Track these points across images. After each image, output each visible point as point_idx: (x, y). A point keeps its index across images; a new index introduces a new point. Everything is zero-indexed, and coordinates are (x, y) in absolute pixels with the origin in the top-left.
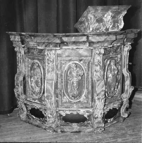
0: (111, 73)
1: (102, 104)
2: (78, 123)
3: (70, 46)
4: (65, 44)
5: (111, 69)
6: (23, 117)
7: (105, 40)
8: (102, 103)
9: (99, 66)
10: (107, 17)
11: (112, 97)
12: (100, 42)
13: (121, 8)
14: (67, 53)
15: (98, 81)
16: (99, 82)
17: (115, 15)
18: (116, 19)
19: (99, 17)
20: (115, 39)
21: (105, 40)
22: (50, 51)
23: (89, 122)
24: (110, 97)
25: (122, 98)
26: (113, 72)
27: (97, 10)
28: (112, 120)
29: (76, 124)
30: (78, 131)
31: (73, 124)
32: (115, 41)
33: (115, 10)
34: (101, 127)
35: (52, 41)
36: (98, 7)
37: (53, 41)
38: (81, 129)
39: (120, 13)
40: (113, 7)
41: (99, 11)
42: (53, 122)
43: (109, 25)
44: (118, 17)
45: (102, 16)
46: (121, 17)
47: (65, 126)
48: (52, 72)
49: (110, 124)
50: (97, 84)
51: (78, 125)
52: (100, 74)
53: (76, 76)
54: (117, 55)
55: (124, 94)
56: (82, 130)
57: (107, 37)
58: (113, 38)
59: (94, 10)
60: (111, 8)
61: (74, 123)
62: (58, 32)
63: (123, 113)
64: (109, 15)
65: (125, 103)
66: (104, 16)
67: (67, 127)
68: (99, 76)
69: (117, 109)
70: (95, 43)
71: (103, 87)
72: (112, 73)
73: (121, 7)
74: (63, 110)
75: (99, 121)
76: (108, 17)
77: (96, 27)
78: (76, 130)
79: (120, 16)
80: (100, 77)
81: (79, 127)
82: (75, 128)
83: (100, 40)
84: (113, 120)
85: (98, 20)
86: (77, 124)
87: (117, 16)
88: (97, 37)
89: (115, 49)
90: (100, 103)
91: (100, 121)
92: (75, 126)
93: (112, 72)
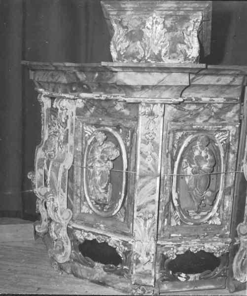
0: (191, 167)
1: (147, 232)
2: (105, 264)
3: (94, 93)
4: (84, 88)
5: (191, 156)
6: (40, 230)
7: (160, 84)
8: (147, 229)
9: (150, 144)
10: (154, 28)
11: (195, 224)
12: (147, 87)
13: (186, 7)
14: (93, 109)
15: (141, 177)
16: (144, 180)
17: (175, 24)
18: (179, 32)
19: (133, 27)
20: (188, 84)
21: (159, 83)
22: (84, 103)
23: (125, 267)
24: (192, 224)
25: (239, 234)
26: (196, 165)
27: (123, 11)
28: (195, 278)
29: (101, 265)
30: (101, 281)
31: (96, 264)
32: (187, 87)
33: (171, 12)
34: (143, 286)
35: (57, 80)
36: (124, 4)
37: (58, 79)
38: (108, 279)
39: (185, 18)
40: (161, 3)
41: (129, 13)
42: (60, 250)
43: (160, 48)
44: (184, 28)
45: (141, 24)
46: (190, 29)
47: (82, 264)
48: (64, 146)
49: (188, 286)
50: (139, 184)
51: (104, 268)
52: (152, 164)
53: (100, 160)
54: (221, 127)
55: (242, 224)
56: (108, 281)
57: (165, 78)
58: (184, 80)
59: (115, 11)
60: (158, 7)
61: (98, 262)
62: (86, 62)
63: (237, 270)
64: (156, 22)
65: (243, 247)
66: (144, 24)
67: (85, 267)
68: (150, 166)
69: (215, 257)
70: (135, 90)
71: (153, 194)
72: (193, 166)
73: (185, 5)
74: (81, 230)
75: (146, 271)
76: (156, 28)
77: (125, 51)
78: (97, 279)
79: (188, 27)
80: (152, 169)
81: (105, 273)
82: (97, 272)
83: (146, 83)
84: (197, 279)
85: (132, 34)
86: (104, 265)
87: (181, 27)
88: (139, 74)
89: (215, 110)
90: (143, 228)
91: (148, 272)
92: (99, 270)
93: (194, 164)
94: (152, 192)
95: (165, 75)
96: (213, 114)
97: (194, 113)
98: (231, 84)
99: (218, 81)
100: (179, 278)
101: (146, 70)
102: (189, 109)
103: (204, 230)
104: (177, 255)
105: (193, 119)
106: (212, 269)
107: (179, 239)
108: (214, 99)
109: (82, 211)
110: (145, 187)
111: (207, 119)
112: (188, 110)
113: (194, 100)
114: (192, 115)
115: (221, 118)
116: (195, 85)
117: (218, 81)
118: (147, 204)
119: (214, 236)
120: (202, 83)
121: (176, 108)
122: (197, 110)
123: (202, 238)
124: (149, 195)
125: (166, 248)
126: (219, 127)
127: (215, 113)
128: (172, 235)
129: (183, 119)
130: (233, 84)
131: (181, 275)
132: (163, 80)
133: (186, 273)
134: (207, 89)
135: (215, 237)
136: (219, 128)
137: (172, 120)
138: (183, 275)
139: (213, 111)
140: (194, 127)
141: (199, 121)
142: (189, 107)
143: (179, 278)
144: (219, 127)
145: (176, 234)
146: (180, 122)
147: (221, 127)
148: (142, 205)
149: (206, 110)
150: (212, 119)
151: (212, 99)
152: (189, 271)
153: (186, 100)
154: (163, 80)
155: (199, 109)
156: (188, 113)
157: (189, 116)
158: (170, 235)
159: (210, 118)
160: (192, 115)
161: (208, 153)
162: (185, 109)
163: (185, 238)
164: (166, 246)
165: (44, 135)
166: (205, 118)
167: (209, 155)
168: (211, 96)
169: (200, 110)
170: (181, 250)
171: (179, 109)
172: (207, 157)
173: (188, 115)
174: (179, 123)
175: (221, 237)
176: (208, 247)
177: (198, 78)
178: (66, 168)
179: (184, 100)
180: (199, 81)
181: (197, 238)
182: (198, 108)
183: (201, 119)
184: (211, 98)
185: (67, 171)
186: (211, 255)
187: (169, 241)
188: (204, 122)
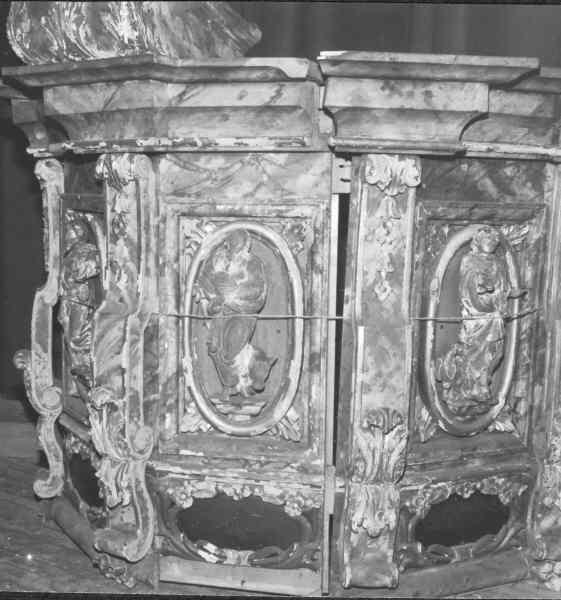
16: (105, 322)
21: (106, 105)
28: (239, 559)
80: (127, 299)
94: (117, 349)
95: (113, 88)
96: (265, 178)
97: (220, 176)
98: (272, 104)
99: (241, 98)
100: (201, 553)
101: (135, 74)
102: (209, 166)
103: (262, 450)
104: (195, 500)
105: (220, 189)
106: (286, 546)
107: (201, 463)
108: (244, 141)
109: (183, 428)
110: (107, 336)
111: (250, 189)
112: (206, 170)
113: (200, 143)
114: (215, 180)
115: (286, 187)
116: (192, 110)
117: (241, 98)
118: (109, 375)
119: (285, 467)
120: (204, 103)
121: (179, 165)
122: (227, 168)
123: (257, 467)
124: (112, 354)
125: (173, 479)
126: (279, 208)
127: (269, 177)
128: (183, 452)
129: (194, 190)
130: (279, 102)
131: (205, 547)
132: (111, 99)
133: (220, 545)
134: (226, 118)
135: (289, 469)
136: (281, 212)
137: (171, 191)
138: (211, 547)
139: (264, 172)
140: (218, 207)
141: (231, 193)
142: (208, 161)
143: (201, 553)
144: (279, 208)
145: (193, 450)
146: (189, 196)
147: (283, 208)
148: (102, 376)
149: (249, 169)
150: (264, 189)
151: (239, 141)
152: (224, 542)
153: (183, 144)
154: (111, 99)
155: (232, 166)
156: (205, 176)
157: (208, 183)
158: (178, 450)
159: (258, 187)
160: (215, 180)
161: (244, 269)
162: (198, 168)
163: (217, 462)
164: (171, 475)
165: (351, 239)
166: (248, 187)
167: (246, 273)
168: (242, 134)
169: (232, 170)
170: (207, 489)
171: (184, 167)
172: (241, 276)
173: (208, 179)
174: (185, 199)
175: (304, 470)
176: (270, 491)
177: (195, 91)
178: (47, 301)
179: (175, 145)
180: (196, 99)
181: (243, 467)
182: (228, 165)
183: (236, 190)
184: (238, 138)
185: (50, 309)
186: (275, 511)
187: (176, 465)
188: (245, 196)
